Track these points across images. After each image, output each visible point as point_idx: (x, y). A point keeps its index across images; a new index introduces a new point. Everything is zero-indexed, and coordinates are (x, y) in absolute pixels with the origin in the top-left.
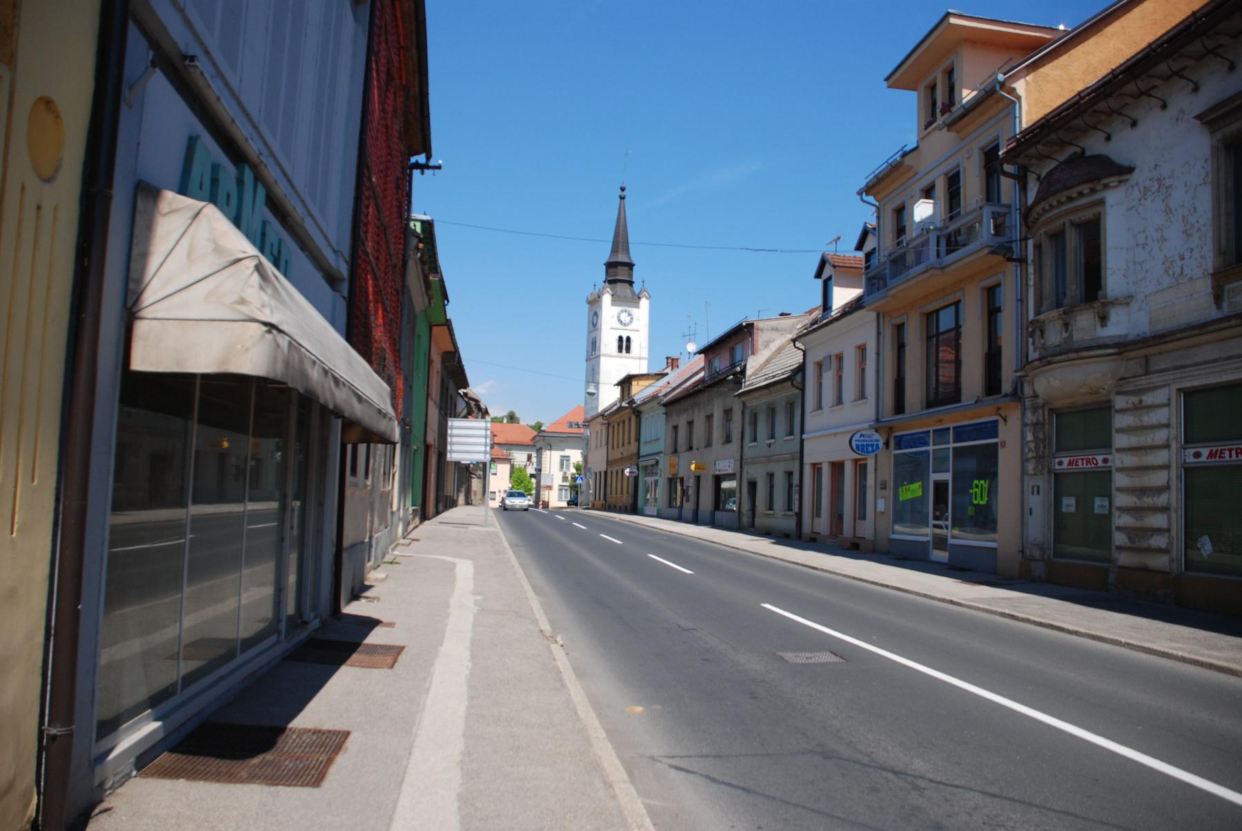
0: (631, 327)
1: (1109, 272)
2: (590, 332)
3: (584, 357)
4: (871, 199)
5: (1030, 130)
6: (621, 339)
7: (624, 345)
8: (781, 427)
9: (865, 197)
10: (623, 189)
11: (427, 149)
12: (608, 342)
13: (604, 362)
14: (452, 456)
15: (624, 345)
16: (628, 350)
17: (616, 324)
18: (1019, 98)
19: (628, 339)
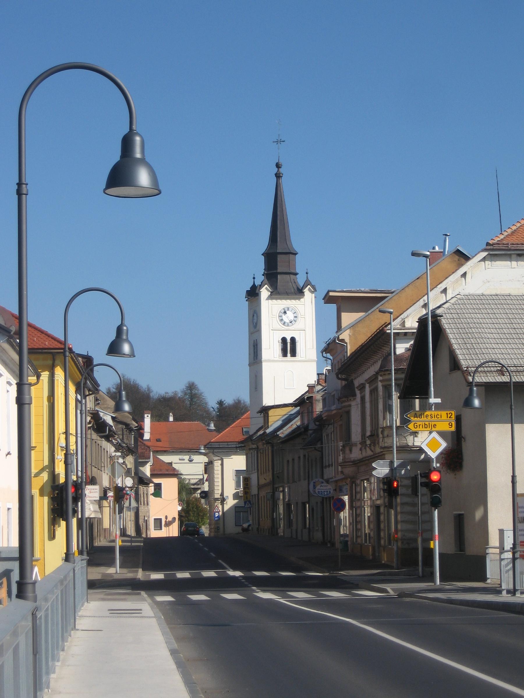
0: (296, 326)
1: (86, 504)
2: (251, 333)
3: (247, 362)
4: (329, 355)
5: (354, 354)
6: (284, 340)
7: (289, 348)
8: (336, 442)
9: (325, 355)
10: (278, 166)
11: (205, 465)
12: (270, 348)
13: (266, 367)
14: (245, 457)
15: (289, 348)
16: (294, 354)
17: (278, 325)
18: (346, 343)
19: (293, 340)
